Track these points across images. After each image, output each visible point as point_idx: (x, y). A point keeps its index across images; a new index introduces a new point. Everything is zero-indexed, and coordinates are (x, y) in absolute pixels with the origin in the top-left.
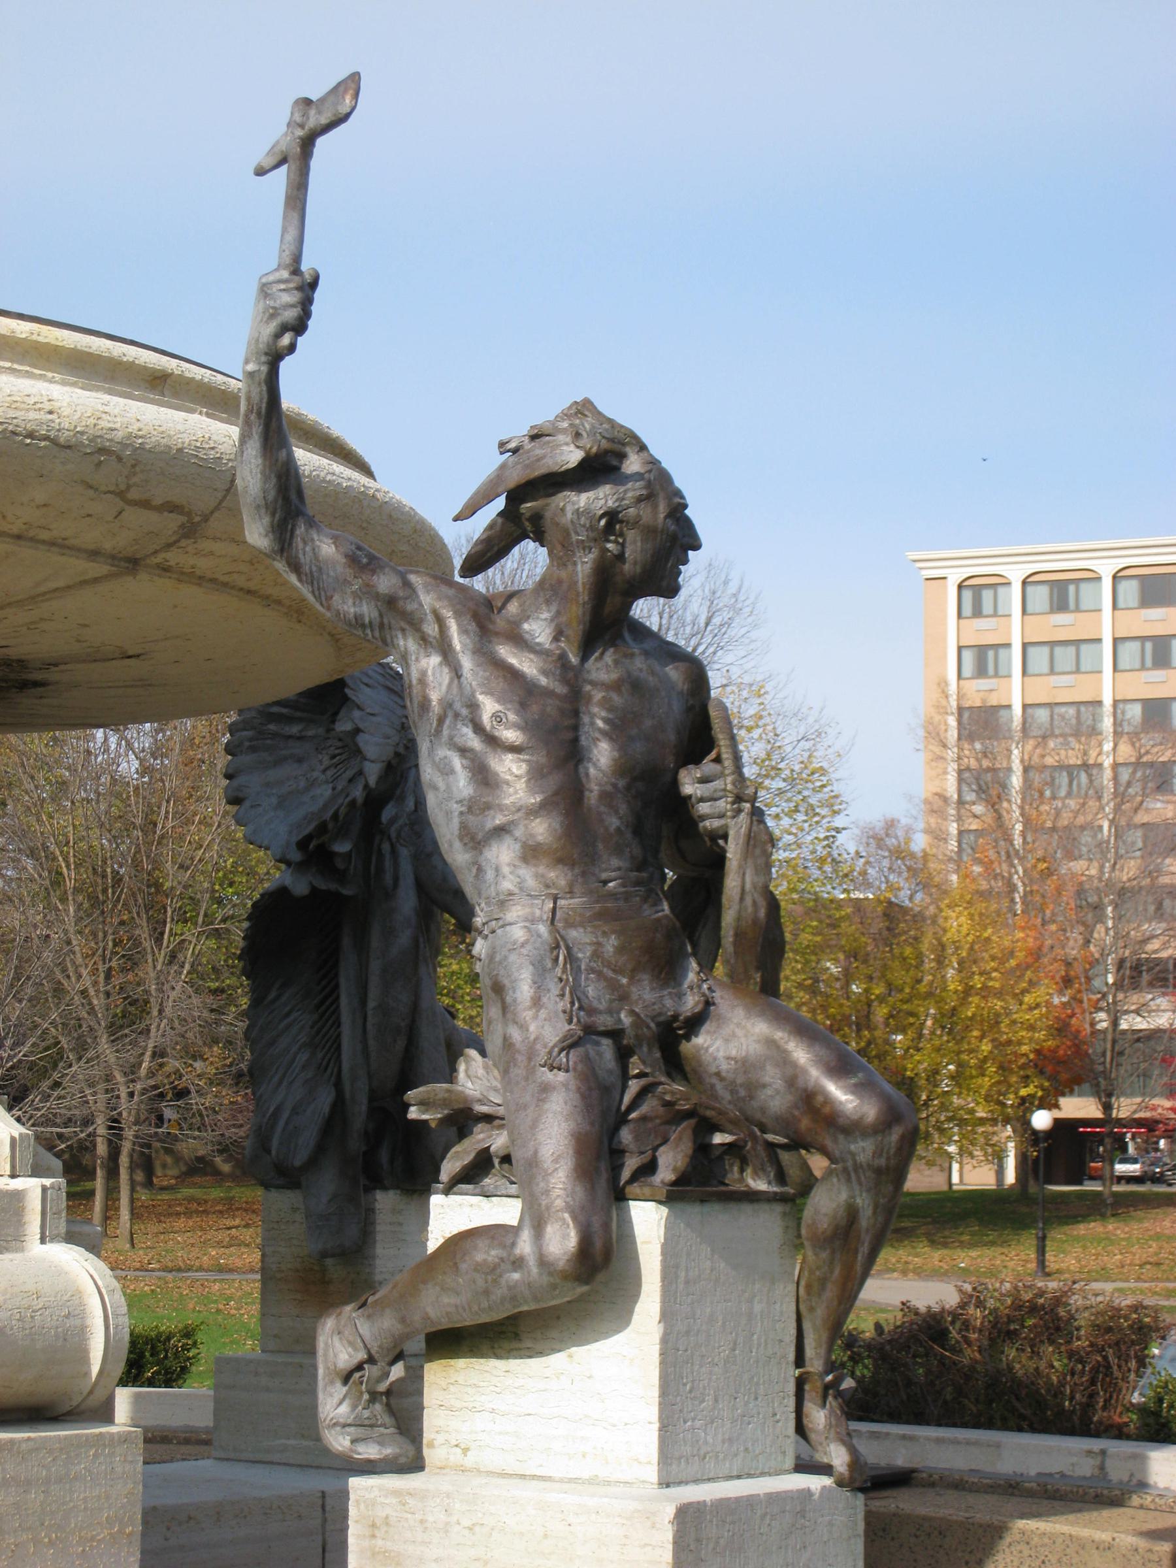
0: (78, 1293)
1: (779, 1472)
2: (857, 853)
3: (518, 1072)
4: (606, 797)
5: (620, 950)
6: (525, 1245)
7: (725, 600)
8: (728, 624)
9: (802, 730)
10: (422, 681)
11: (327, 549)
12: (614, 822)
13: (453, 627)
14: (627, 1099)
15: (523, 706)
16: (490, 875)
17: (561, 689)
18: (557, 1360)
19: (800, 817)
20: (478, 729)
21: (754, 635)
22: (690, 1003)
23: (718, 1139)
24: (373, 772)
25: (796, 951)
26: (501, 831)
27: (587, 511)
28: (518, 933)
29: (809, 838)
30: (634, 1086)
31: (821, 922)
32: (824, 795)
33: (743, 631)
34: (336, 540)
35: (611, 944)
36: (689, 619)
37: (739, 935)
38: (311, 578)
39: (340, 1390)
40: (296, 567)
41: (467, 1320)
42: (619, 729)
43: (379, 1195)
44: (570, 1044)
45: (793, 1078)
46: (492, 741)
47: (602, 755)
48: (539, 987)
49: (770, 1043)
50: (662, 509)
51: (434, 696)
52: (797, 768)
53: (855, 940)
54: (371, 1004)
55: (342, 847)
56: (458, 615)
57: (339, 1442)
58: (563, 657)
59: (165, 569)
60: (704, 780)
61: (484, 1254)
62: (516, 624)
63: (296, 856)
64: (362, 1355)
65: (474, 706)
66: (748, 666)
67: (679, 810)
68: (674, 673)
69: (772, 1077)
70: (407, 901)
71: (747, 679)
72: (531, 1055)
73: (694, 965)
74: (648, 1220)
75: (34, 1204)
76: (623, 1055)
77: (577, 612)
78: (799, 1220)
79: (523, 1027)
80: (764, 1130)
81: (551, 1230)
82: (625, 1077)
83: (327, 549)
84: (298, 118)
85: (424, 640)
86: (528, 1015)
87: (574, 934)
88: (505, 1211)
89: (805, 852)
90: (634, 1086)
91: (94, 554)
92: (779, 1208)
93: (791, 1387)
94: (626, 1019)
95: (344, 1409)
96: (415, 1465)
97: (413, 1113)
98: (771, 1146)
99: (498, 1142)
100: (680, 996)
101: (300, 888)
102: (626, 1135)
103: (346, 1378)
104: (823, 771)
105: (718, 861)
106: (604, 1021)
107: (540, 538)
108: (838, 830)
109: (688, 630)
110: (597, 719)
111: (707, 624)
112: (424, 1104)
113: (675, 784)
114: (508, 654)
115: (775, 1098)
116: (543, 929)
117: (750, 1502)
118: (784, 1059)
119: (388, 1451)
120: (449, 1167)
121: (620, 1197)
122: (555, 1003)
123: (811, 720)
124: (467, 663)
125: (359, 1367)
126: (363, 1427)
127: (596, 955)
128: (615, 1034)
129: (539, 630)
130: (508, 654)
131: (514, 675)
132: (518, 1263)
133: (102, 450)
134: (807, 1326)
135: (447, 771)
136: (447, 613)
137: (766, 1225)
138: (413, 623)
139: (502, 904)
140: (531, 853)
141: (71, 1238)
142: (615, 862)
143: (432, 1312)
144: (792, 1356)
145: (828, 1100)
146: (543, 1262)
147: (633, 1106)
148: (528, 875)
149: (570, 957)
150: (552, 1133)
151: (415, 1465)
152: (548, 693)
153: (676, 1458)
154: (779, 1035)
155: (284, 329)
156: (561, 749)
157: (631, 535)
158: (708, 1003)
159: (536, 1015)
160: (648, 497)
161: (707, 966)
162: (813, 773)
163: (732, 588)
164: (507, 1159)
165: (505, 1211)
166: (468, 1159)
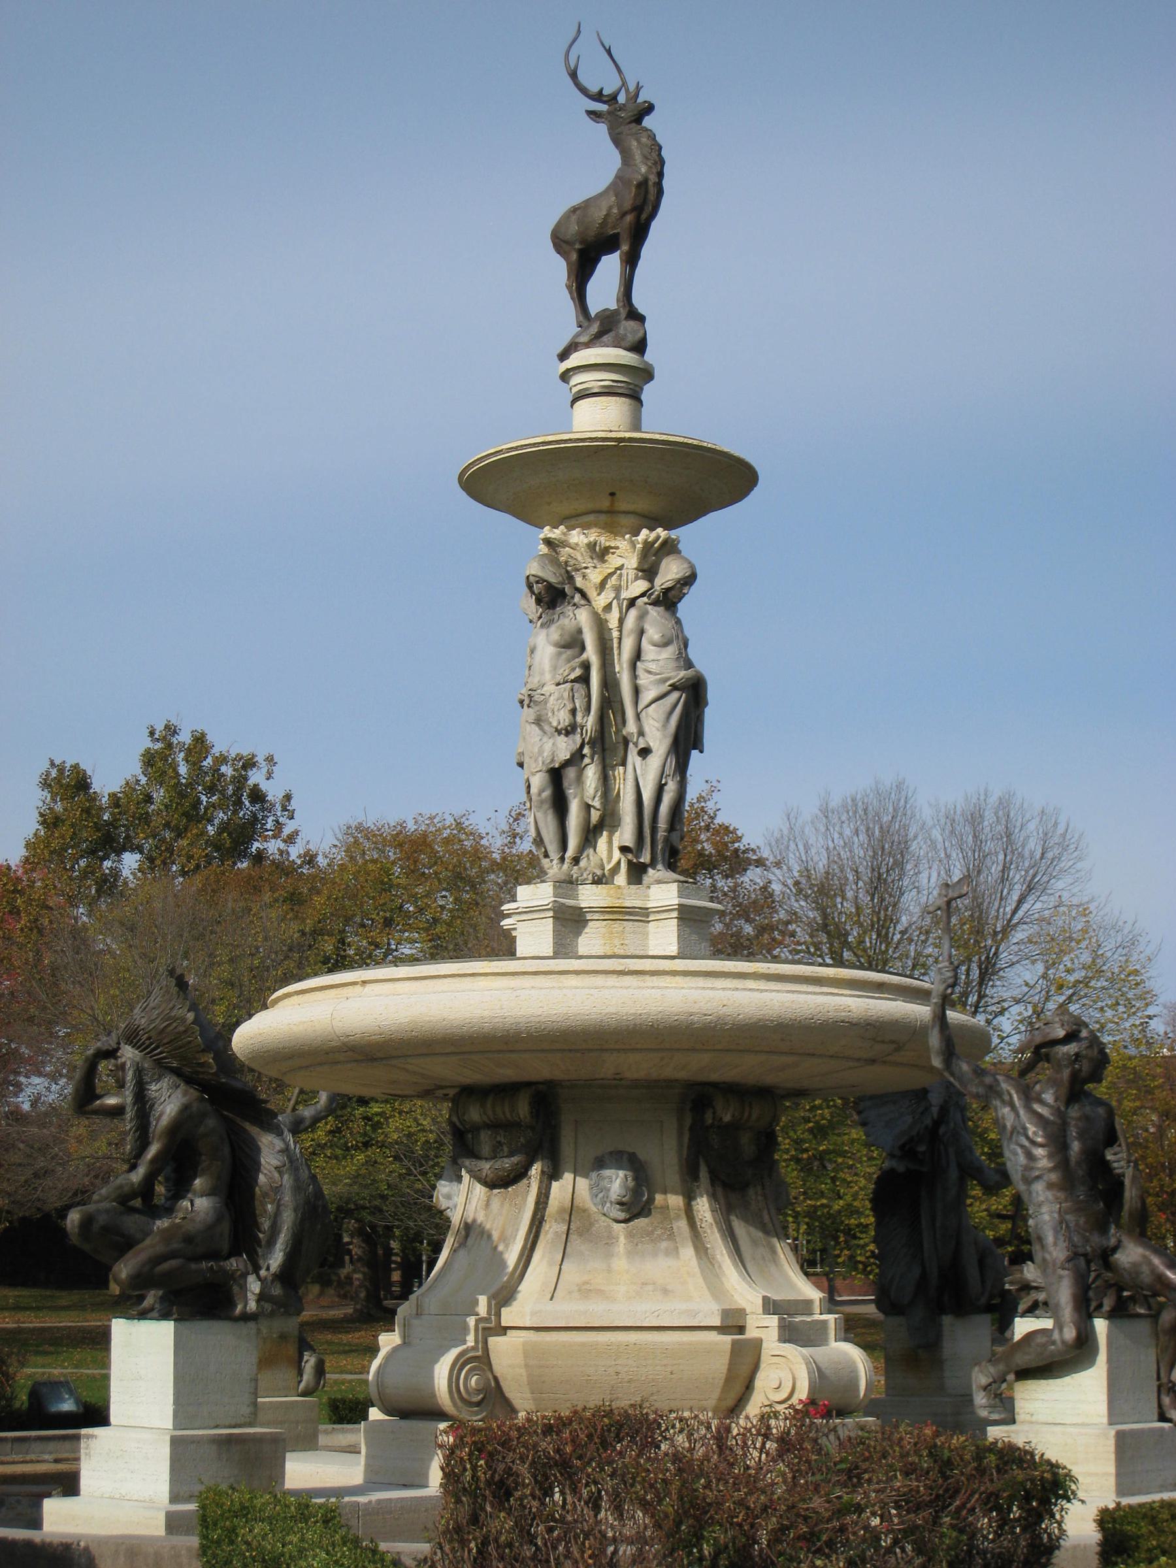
0: (854, 1362)
1: (1152, 1421)
2: (1166, 1033)
3: (1049, 1271)
4: (1078, 1163)
5: (1085, 1223)
6: (1056, 1336)
7: (1056, 839)
8: (1058, 858)
9: (1119, 939)
10: (1003, 1118)
11: (965, 1067)
12: (1081, 1173)
13: (1015, 1096)
14: (1091, 1280)
15: (1044, 1129)
16: (1034, 1195)
17: (1059, 1121)
18: (1067, 1379)
19: (1121, 1009)
20: (1028, 1138)
21: (1079, 865)
22: (1113, 1242)
23: (1125, 1294)
24: (935, 1111)
25: (1121, 1116)
26: (1038, 1178)
27: (1067, 1054)
28: (1047, 1217)
29: (1127, 1025)
30: (1093, 1275)
31: (1139, 1089)
32: (1138, 991)
33: (1070, 863)
34: (968, 1063)
35: (1082, 1221)
36: (1027, 853)
37: (1131, 1214)
38: (960, 1080)
39: (982, 1394)
40: (952, 1074)
41: (1034, 1365)
42: (1081, 1136)
43: (944, 1317)
44: (1069, 1260)
45: (1153, 1270)
46: (1033, 1143)
47: (1076, 1146)
48: (1056, 1238)
49: (1144, 1257)
50: (1096, 1051)
51: (1009, 1125)
52: (1116, 970)
53: (1167, 1104)
54: (938, 1224)
55: (922, 1148)
56: (1017, 1092)
57: (984, 1413)
58: (1059, 1108)
59: (885, 1062)
60: (1115, 1154)
61: (1041, 1340)
62: (1039, 1094)
63: (897, 1153)
64: (991, 1380)
65: (1025, 1129)
66: (1075, 890)
67: (1105, 1166)
68: (1101, 1110)
69: (1145, 1269)
70: (953, 1174)
71: (1075, 901)
72: (1054, 1265)
73: (1113, 1226)
74: (1101, 1326)
75: (832, 1325)
76: (1088, 1262)
77: (1064, 1091)
78: (1157, 1323)
79: (1050, 1253)
80: (1142, 1289)
81: (1065, 1330)
82: (1089, 1271)
83: (965, 1067)
84: (944, 892)
85: (1003, 1102)
86: (1051, 1249)
87: (1068, 1217)
88: (1048, 1323)
89: (1126, 1036)
90: (1093, 1275)
91: (858, 1060)
92: (1149, 1320)
93: (1155, 1389)
94: (1088, 1248)
95: (984, 1401)
96: (1013, 1422)
97: (1007, 1287)
98: (1146, 1296)
99: (1042, 1297)
100: (1108, 1239)
101: (901, 1168)
102: (1091, 1294)
103: (985, 1388)
104: (1136, 972)
105: (1121, 1184)
106: (1081, 1250)
107: (1048, 1061)
108: (1150, 1017)
109: (1027, 864)
110: (1073, 1132)
111: (1042, 858)
112: (1011, 1283)
113: (1103, 1156)
114: (1037, 1107)
115: (1146, 1277)
116: (1056, 1215)
117: (1142, 1431)
118: (1150, 1263)
119: (1003, 1416)
120: (1021, 1307)
121: (1090, 1317)
122: (1063, 1244)
123: (1126, 932)
124: (1022, 1112)
125: (990, 1385)
126: (992, 1407)
127: (1077, 1225)
128: (1085, 1255)
129: (1049, 1097)
130: (1037, 1107)
131: (1040, 1116)
132: (1054, 1343)
133: (869, 1024)
134: (1161, 1365)
135: (1016, 1154)
136: (1013, 1092)
137: (1144, 1327)
138: (999, 1094)
139: (1040, 1205)
140: (1050, 1186)
141: (846, 1340)
142: (1082, 1188)
143: (1019, 1362)
144: (1155, 1376)
145: (1168, 1278)
146: (1063, 1342)
147: (1093, 1282)
148: (1050, 1195)
149: (1067, 1226)
150: (1064, 1294)
151: (1013, 1422)
152: (1053, 1123)
153: (1114, 1415)
154: (1147, 1253)
155: (949, 986)
156: (1058, 1142)
157: (1085, 1062)
158: (1120, 1241)
159: (1054, 1248)
160: (1090, 1047)
161: (1118, 1226)
162: (1129, 975)
163: (1061, 829)
164: (1046, 1304)
165: (1048, 1323)
166: (1030, 1304)
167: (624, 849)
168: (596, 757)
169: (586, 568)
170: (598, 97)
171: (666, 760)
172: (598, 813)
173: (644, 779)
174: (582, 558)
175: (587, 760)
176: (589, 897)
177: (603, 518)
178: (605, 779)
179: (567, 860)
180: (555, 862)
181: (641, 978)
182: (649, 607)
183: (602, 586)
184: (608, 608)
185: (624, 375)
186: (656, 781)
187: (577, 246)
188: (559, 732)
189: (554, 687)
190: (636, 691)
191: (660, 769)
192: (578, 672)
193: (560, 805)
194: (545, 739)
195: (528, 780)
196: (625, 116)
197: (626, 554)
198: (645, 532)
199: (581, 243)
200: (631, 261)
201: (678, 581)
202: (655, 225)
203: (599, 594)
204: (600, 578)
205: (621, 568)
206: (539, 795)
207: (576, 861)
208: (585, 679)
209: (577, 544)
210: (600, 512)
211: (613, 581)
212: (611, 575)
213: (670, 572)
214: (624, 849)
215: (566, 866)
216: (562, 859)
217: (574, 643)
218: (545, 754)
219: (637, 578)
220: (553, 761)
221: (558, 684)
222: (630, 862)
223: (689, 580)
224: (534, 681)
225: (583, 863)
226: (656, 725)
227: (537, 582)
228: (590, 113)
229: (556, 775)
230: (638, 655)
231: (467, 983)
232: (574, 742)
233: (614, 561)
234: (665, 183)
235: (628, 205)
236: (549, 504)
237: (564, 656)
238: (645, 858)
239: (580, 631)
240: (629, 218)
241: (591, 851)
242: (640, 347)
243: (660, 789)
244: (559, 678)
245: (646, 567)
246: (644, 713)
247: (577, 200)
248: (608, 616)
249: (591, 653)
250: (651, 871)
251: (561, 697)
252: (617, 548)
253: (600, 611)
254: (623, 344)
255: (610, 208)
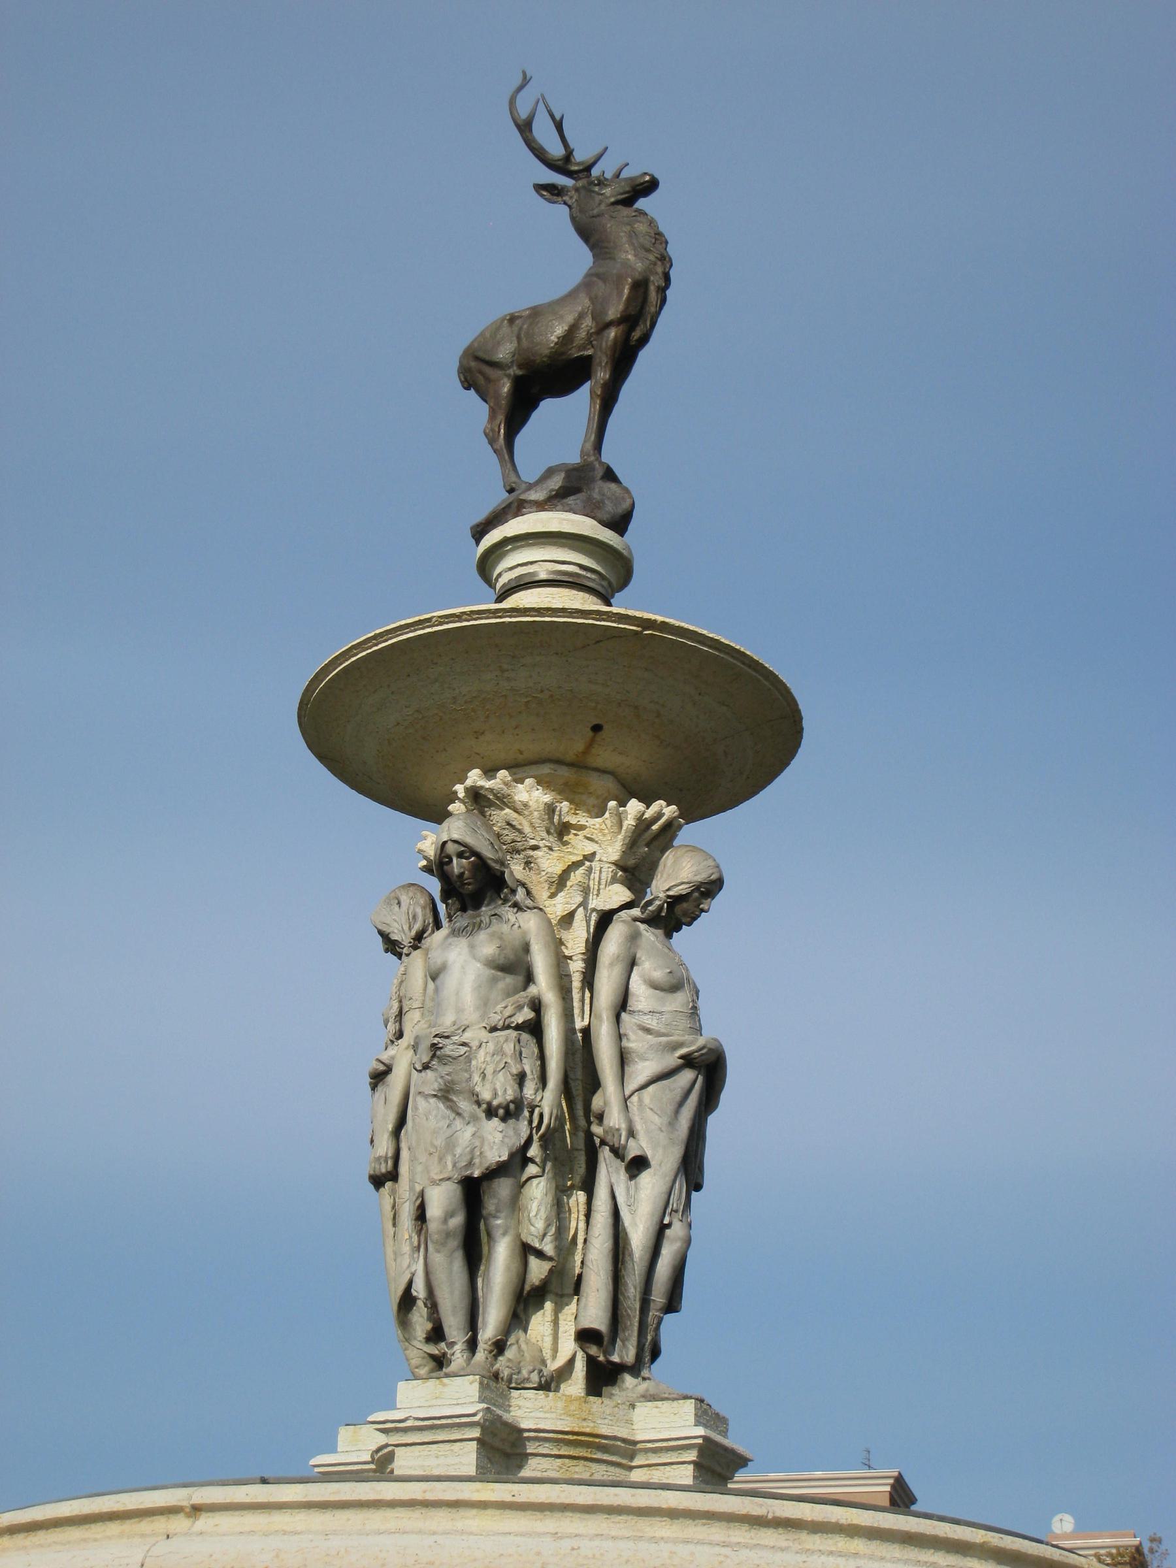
167: (585, 1336)
168: (549, 1165)
169: (535, 848)
170: (562, 166)
171: (674, 1182)
172: (546, 1266)
173: (633, 1213)
174: (533, 830)
175: (532, 1169)
176: (530, 1411)
177: (564, 772)
178: (559, 1209)
179: (482, 1346)
180: (458, 1347)
181: (793, 1535)
182: (642, 927)
183: (561, 882)
184: (568, 919)
185: (598, 563)
186: (656, 1219)
187: (515, 371)
188: (491, 1112)
189: (484, 1035)
190: (623, 1059)
191: (665, 1196)
192: (526, 1014)
193: (473, 1250)
194: (458, 1123)
195: (422, 1194)
196: (600, 201)
197: (603, 837)
198: (634, 806)
199: (520, 367)
200: (608, 400)
201: (697, 887)
202: (644, 356)
203: (553, 896)
204: (558, 869)
205: (590, 857)
206: (445, 1221)
207: (499, 1347)
208: (535, 1028)
209: (526, 805)
210: (559, 762)
211: (577, 876)
212: (576, 865)
213: (675, 873)
214: (585, 1336)
215: (481, 1355)
216: (472, 1345)
217: (514, 967)
218: (458, 1151)
219: (614, 880)
220: (470, 1164)
221: (494, 1029)
222: (591, 1361)
223: (710, 888)
224: (447, 1021)
225: (510, 1353)
226: (657, 1120)
227: (460, 855)
228: (539, 188)
229: (473, 1191)
230: (622, 1004)
231: (440, 1519)
232: (517, 1132)
233: (579, 845)
234: (669, 293)
235: (614, 311)
236: (478, 734)
237: (501, 985)
238: (625, 1353)
239: (526, 948)
240: (612, 333)
241: (521, 1333)
242: (620, 524)
243: (661, 1229)
244: (496, 1019)
245: (631, 862)
246: (635, 1098)
247: (521, 304)
248: (565, 935)
249: (544, 985)
250: (628, 1380)
251: (499, 1051)
252: (582, 828)
253: (554, 922)
254: (599, 515)
255: (581, 316)
